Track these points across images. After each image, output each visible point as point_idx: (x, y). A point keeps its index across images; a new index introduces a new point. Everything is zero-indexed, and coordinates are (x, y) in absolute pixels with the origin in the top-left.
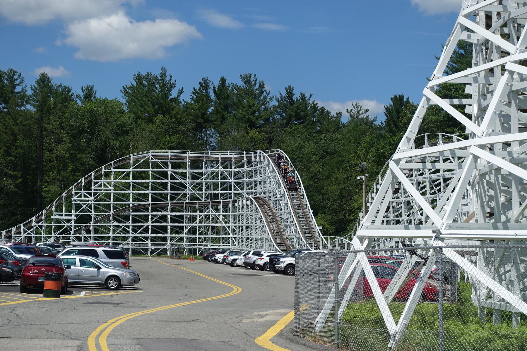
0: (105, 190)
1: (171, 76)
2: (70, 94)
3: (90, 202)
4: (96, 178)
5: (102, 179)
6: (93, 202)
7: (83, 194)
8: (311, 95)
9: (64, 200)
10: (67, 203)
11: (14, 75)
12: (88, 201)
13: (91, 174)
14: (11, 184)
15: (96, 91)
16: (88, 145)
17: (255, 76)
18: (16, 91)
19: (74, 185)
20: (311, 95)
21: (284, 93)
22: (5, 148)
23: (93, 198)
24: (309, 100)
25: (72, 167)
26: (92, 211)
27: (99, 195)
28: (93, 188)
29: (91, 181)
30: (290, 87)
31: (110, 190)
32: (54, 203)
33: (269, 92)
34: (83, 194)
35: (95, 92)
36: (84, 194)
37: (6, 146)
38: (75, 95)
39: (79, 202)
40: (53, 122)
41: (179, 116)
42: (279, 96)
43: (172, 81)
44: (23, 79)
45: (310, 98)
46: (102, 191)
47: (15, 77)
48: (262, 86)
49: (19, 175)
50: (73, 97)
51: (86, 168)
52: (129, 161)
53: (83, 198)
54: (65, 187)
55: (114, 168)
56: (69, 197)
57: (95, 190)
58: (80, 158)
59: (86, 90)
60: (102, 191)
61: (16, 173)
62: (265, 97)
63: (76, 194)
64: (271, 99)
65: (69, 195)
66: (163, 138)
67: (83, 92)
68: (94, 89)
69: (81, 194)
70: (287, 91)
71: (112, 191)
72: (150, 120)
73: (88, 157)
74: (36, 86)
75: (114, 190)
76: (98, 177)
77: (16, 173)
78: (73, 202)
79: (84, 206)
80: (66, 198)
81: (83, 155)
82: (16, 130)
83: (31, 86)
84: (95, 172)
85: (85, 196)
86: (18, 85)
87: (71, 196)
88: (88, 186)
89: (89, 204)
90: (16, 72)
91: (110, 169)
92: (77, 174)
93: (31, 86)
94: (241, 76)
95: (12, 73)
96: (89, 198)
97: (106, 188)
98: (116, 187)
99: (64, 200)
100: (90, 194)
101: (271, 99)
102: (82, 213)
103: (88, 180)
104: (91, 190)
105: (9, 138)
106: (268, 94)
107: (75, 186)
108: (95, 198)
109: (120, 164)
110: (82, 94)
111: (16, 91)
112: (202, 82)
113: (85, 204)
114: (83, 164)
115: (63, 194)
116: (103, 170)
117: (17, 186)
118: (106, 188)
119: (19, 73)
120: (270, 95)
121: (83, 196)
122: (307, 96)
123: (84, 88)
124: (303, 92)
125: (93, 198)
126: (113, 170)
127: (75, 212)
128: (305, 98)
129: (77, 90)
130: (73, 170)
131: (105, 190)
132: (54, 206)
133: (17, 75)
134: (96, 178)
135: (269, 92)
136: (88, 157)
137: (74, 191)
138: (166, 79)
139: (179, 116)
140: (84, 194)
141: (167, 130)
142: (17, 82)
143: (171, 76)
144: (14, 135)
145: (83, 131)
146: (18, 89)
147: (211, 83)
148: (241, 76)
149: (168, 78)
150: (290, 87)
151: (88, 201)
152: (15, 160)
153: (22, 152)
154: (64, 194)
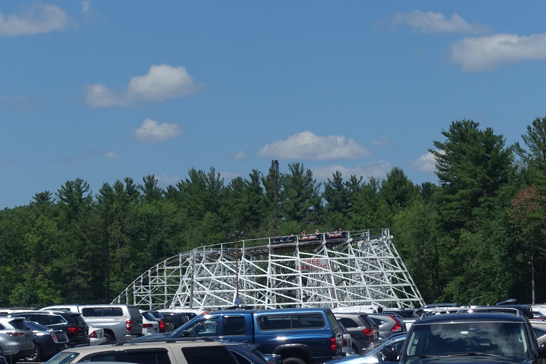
0: (160, 284)
1: (219, 175)
2: (133, 185)
3: (147, 295)
4: (152, 275)
5: (156, 275)
6: (150, 295)
7: (142, 289)
8: (362, 178)
9: (127, 294)
10: (129, 296)
11: (80, 183)
12: (146, 294)
13: (148, 272)
14: (84, 282)
15: (157, 180)
16: (148, 240)
17: (302, 165)
18: (83, 197)
19: (142, 275)
20: (362, 178)
21: (332, 179)
22: (77, 252)
23: (150, 291)
24: (359, 182)
25: (133, 265)
26: (151, 302)
27: (156, 288)
28: (149, 283)
29: (148, 278)
30: (337, 173)
31: (164, 284)
32: (119, 297)
33: (315, 180)
34: (142, 289)
35: (156, 181)
36: (143, 289)
37: (77, 250)
38: (137, 185)
39: (139, 295)
40: (115, 231)
41: (224, 214)
42: (327, 182)
43: (220, 179)
44: (89, 186)
45: (361, 180)
46: (157, 286)
47: (82, 185)
48: (309, 173)
49: (90, 274)
50: (135, 188)
51: (145, 264)
52: (178, 260)
53: (142, 292)
54: (128, 282)
55: (167, 266)
56: (131, 291)
57: (152, 285)
58: (140, 256)
59: (147, 180)
60: (157, 286)
61: (87, 272)
62: (312, 186)
63: (152, 279)
64: (319, 185)
65: (131, 290)
66: (209, 236)
67: (145, 182)
68: (155, 179)
69: (141, 289)
70: (334, 176)
71: (165, 285)
72: (201, 217)
73: (147, 254)
74: (100, 194)
75: (167, 284)
76: (154, 274)
77: (87, 272)
78: (134, 295)
79: (143, 298)
80: (129, 292)
81: (143, 253)
82: (84, 236)
83: (96, 194)
84: (152, 270)
85: (144, 290)
86: (85, 191)
87: (132, 290)
88: (146, 282)
89: (147, 296)
90: (82, 180)
91: (163, 267)
92: (137, 270)
93: (96, 194)
94: (289, 166)
95: (79, 181)
96: (147, 291)
97: (160, 283)
98: (169, 282)
99: (127, 294)
100: (148, 288)
101: (319, 185)
102: (141, 304)
103: (145, 277)
104: (148, 285)
105: (80, 243)
106: (314, 182)
107: (135, 282)
108: (152, 291)
109: (172, 262)
110: (143, 184)
111: (83, 197)
112: (252, 173)
113: (143, 297)
114: (143, 260)
115: (126, 289)
116: (157, 268)
117: (88, 283)
118: (160, 283)
119: (85, 182)
120: (318, 182)
121: (142, 290)
122: (358, 178)
123: (145, 178)
124: (353, 175)
125: (150, 291)
126: (165, 268)
127: (137, 303)
128: (356, 180)
129: (139, 182)
130: (134, 267)
131: (160, 284)
132: (119, 299)
133: (84, 183)
134: (152, 275)
135: (315, 180)
136: (147, 254)
137: (134, 286)
138: (215, 177)
139: (224, 214)
140: (143, 289)
141: (213, 229)
142: (84, 189)
143: (219, 175)
144: (82, 239)
145: (142, 230)
146: (85, 195)
147: (261, 174)
148: (289, 166)
149: (216, 176)
150: (337, 173)
151: (146, 294)
152: (86, 261)
153: (91, 254)
154: (127, 289)
